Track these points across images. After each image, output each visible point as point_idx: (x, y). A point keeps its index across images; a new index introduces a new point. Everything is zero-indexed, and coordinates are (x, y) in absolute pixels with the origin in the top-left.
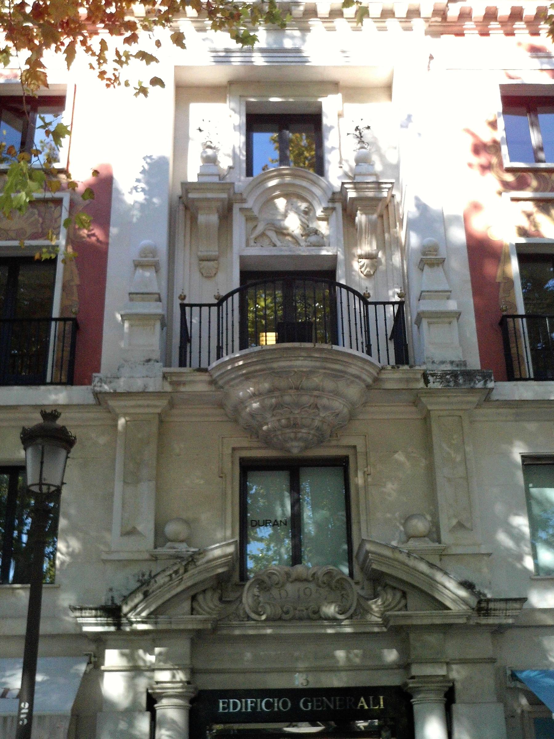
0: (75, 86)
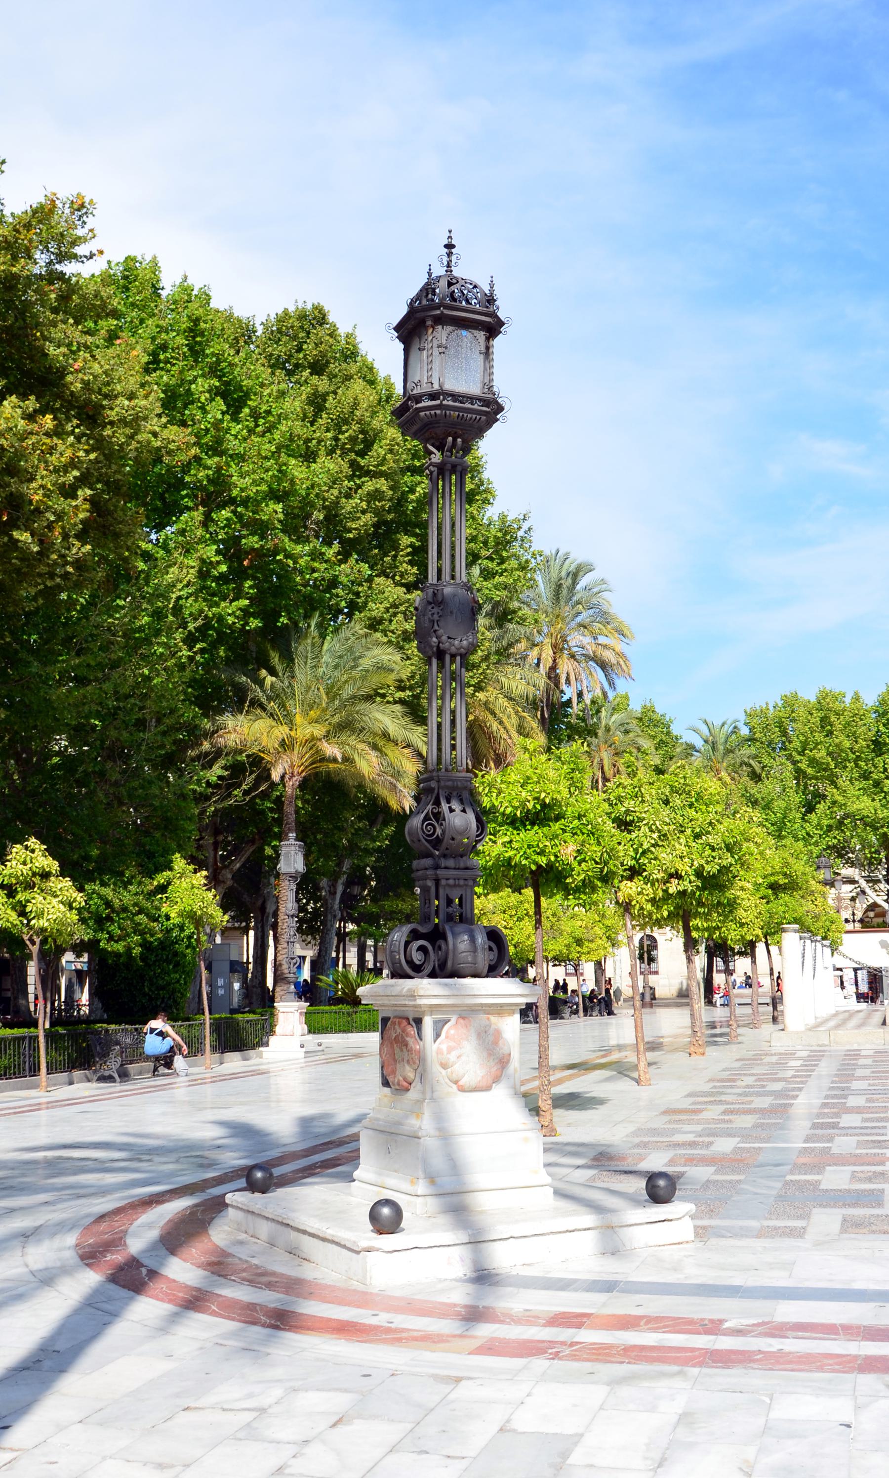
0: (370, 1375)
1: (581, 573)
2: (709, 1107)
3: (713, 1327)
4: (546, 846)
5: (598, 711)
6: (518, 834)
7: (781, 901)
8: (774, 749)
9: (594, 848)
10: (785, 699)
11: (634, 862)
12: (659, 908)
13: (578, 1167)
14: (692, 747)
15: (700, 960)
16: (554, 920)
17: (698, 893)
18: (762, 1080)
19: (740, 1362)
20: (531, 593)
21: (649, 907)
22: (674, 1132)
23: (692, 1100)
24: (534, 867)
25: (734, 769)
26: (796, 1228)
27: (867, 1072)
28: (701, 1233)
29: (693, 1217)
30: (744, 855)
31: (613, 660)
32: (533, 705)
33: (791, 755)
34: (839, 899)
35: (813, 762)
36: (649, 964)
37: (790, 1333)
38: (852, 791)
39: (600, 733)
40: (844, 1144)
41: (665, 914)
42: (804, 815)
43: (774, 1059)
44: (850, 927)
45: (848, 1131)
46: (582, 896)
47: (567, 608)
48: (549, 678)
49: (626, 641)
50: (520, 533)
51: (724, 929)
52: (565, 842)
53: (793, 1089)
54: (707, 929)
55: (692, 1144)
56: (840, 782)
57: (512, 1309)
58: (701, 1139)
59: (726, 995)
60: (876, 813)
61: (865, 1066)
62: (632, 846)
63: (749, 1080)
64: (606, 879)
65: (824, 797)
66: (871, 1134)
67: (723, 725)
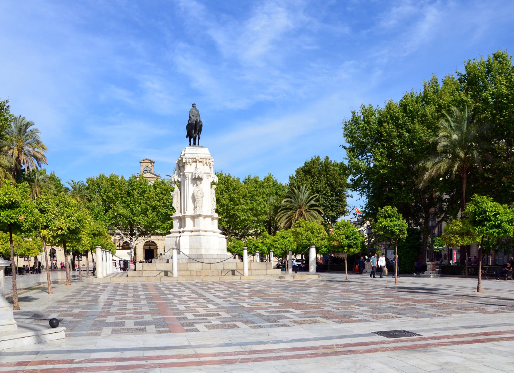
1: (29, 125)
2: (72, 300)
3: (71, 362)
4: (13, 216)
5: (35, 174)
6: (3, 212)
7: (96, 239)
8: (95, 192)
9: (31, 218)
10: (100, 176)
11: (46, 224)
12: (55, 239)
13: (27, 319)
14: (68, 189)
15: (70, 257)
16: (19, 242)
17: (68, 235)
18: (89, 292)
19: (79, 370)
20: (8, 129)
21: (52, 239)
22: (60, 307)
23: (66, 298)
24: (9, 223)
25: (82, 197)
26: (98, 333)
27: (122, 290)
28: (67, 336)
29: (65, 331)
30: (84, 224)
31: (40, 157)
32: (10, 169)
33: (101, 194)
34: (115, 240)
35: (108, 197)
36: (53, 258)
37: (94, 361)
38: (120, 207)
39: (35, 181)
40: (113, 310)
41: (57, 241)
42: (105, 213)
43: (93, 286)
44: (118, 248)
45: (115, 306)
46: (27, 233)
47: (23, 137)
48: (16, 160)
49: (45, 151)
50: (5, 107)
51: (77, 247)
52: (21, 215)
53: (99, 295)
54: (72, 247)
55: (66, 311)
56: (116, 204)
57: (2, 363)
58: (69, 309)
59: (79, 267)
60: (127, 214)
61: (121, 288)
62: (45, 218)
63: (85, 292)
64: (36, 228)
65: (111, 208)
66: (122, 307)
67: (78, 182)
